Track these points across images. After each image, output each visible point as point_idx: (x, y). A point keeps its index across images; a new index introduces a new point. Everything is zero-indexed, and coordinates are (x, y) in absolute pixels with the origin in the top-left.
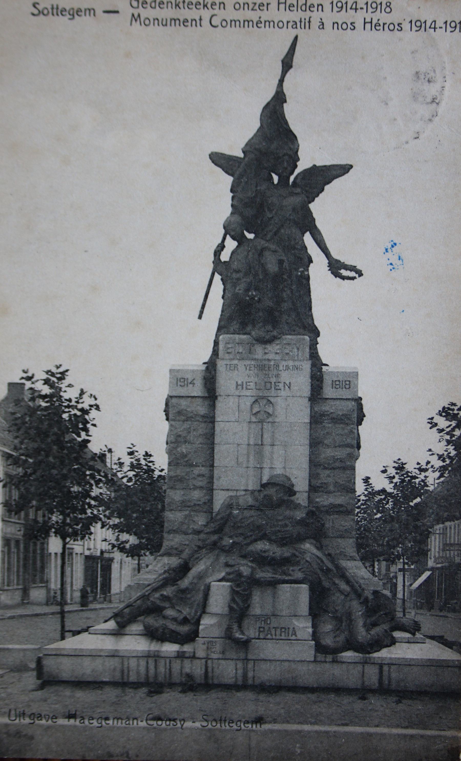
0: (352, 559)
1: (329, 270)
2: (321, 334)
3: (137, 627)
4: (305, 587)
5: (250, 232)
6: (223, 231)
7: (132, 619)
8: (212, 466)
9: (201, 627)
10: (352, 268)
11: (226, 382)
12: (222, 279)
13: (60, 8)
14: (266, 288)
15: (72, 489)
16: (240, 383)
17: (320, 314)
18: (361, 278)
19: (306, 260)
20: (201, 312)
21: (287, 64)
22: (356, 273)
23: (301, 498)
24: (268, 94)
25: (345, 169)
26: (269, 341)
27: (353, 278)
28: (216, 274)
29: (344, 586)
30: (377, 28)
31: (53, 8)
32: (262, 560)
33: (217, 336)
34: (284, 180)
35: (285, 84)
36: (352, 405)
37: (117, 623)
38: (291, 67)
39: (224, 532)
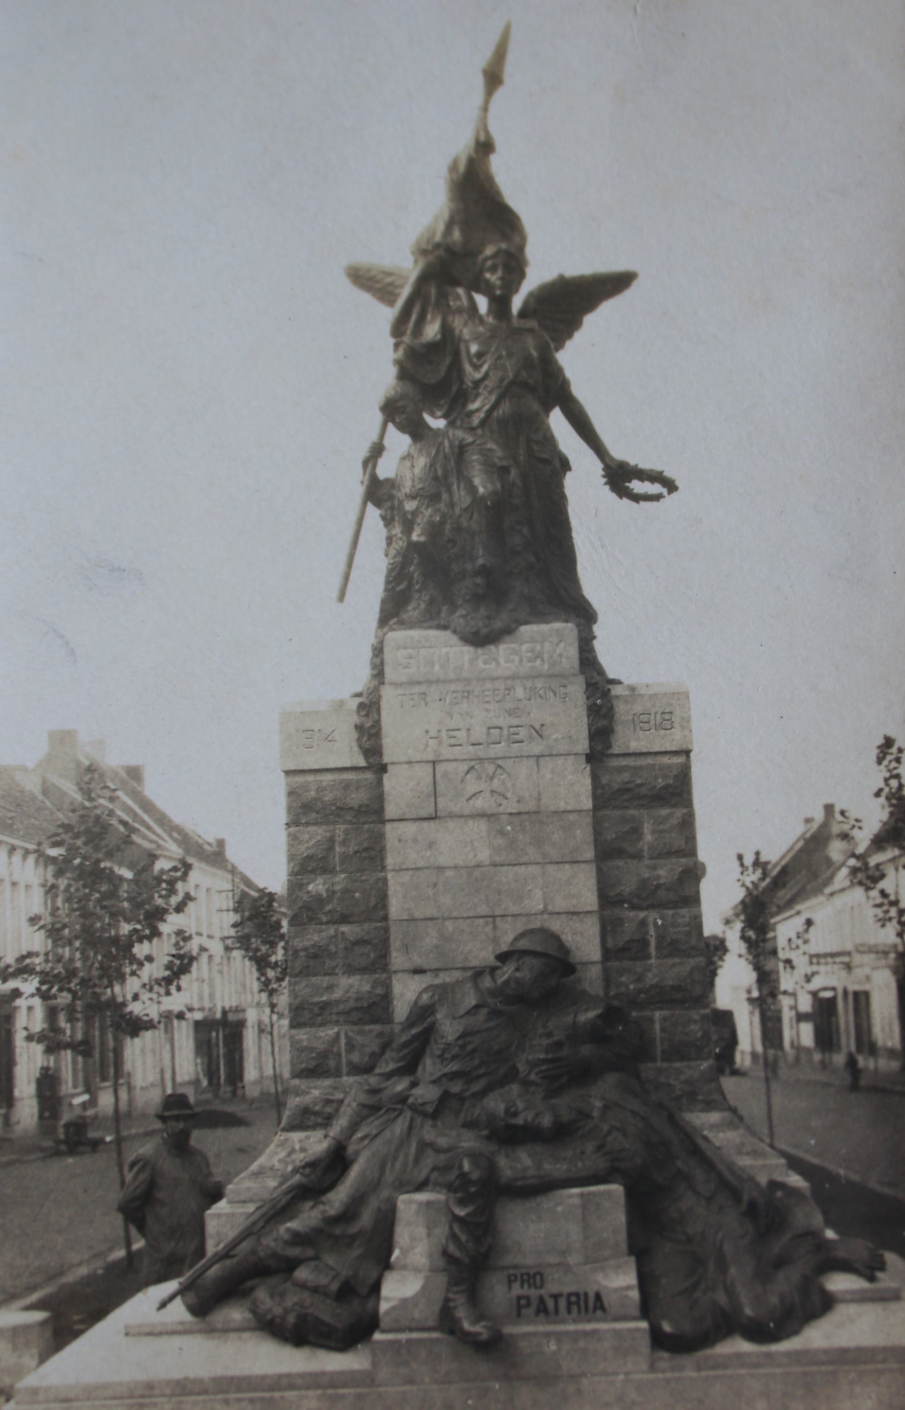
1: (606, 484)
4: (616, 1189)
6: (379, 417)
14: (490, 537)
15: (488, 275)
18: (674, 495)
21: (493, 78)
22: (664, 486)
23: (592, 979)
25: (618, 283)
27: (657, 498)
28: (370, 507)
29: (699, 1175)
32: (510, 1135)
34: (500, 305)
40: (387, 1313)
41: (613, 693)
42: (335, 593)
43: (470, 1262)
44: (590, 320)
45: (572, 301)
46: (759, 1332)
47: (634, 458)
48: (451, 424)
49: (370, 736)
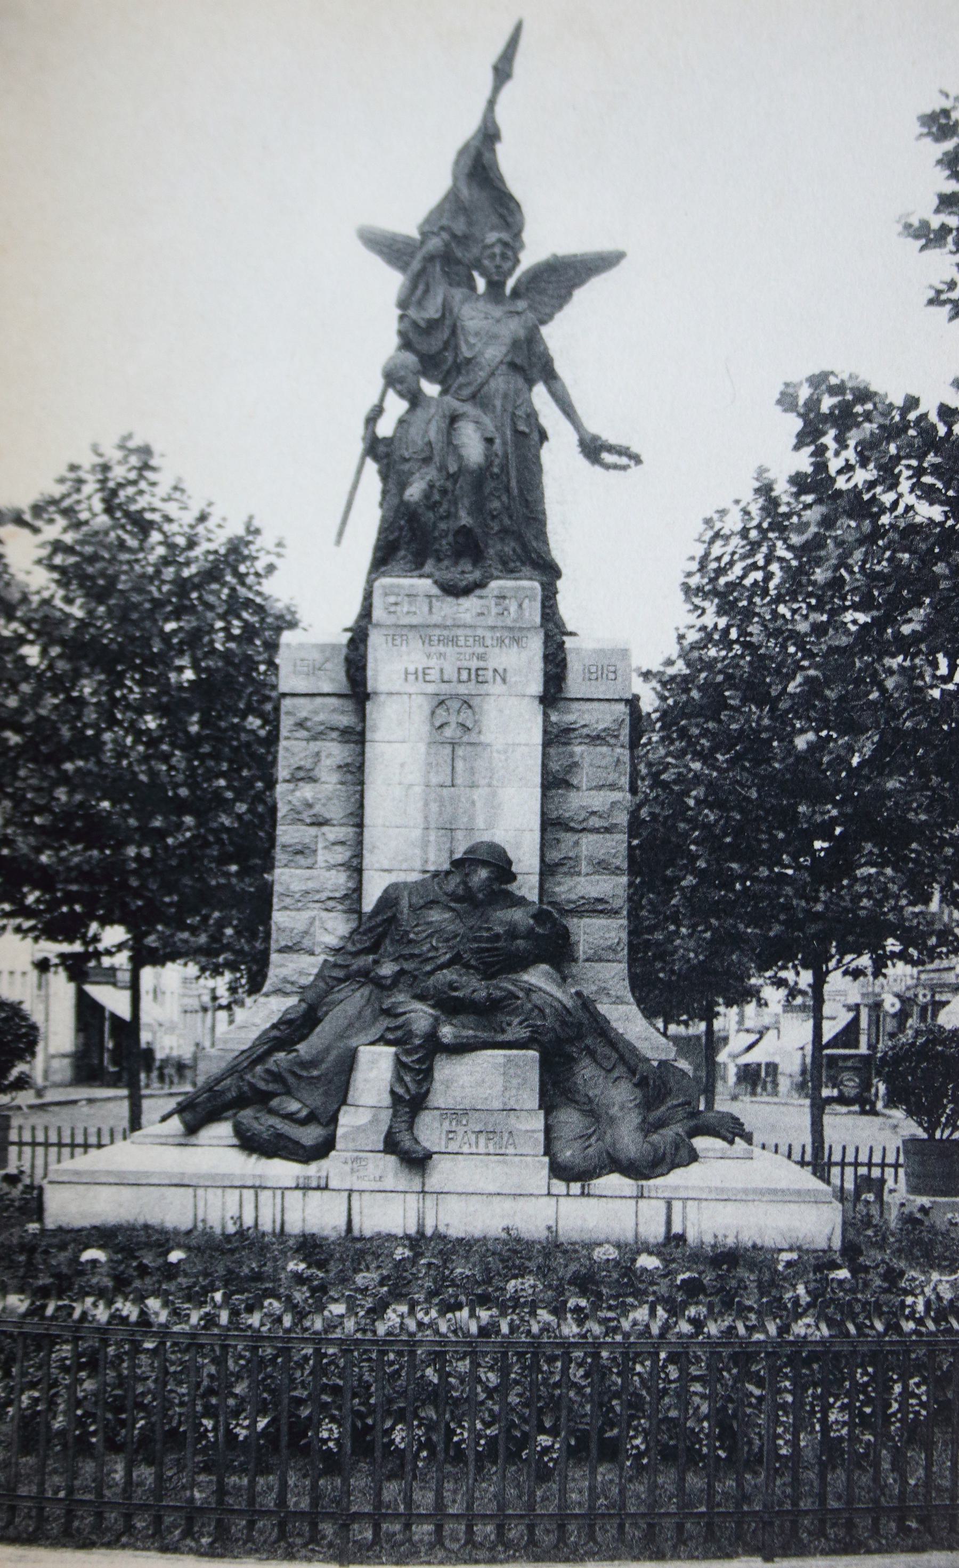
0: (619, 1001)
2: (564, 570)
3: (223, 1130)
6: (380, 382)
7: (213, 1116)
8: (360, 825)
9: (340, 1131)
11: (387, 667)
12: (380, 472)
16: (412, 669)
17: (564, 537)
19: (535, 436)
20: (340, 534)
21: (503, 71)
23: (527, 885)
24: (467, 127)
26: (466, 591)
27: (624, 468)
33: (370, 583)
36: (622, 708)
37: (184, 1122)
39: (382, 951)
40: (345, 1136)
41: (567, 646)
43: (410, 1102)
44: (580, 295)
45: (562, 278)
46: (633, 1170)
47: (610, 436)
48: (444, 392)
49: (358, 669)
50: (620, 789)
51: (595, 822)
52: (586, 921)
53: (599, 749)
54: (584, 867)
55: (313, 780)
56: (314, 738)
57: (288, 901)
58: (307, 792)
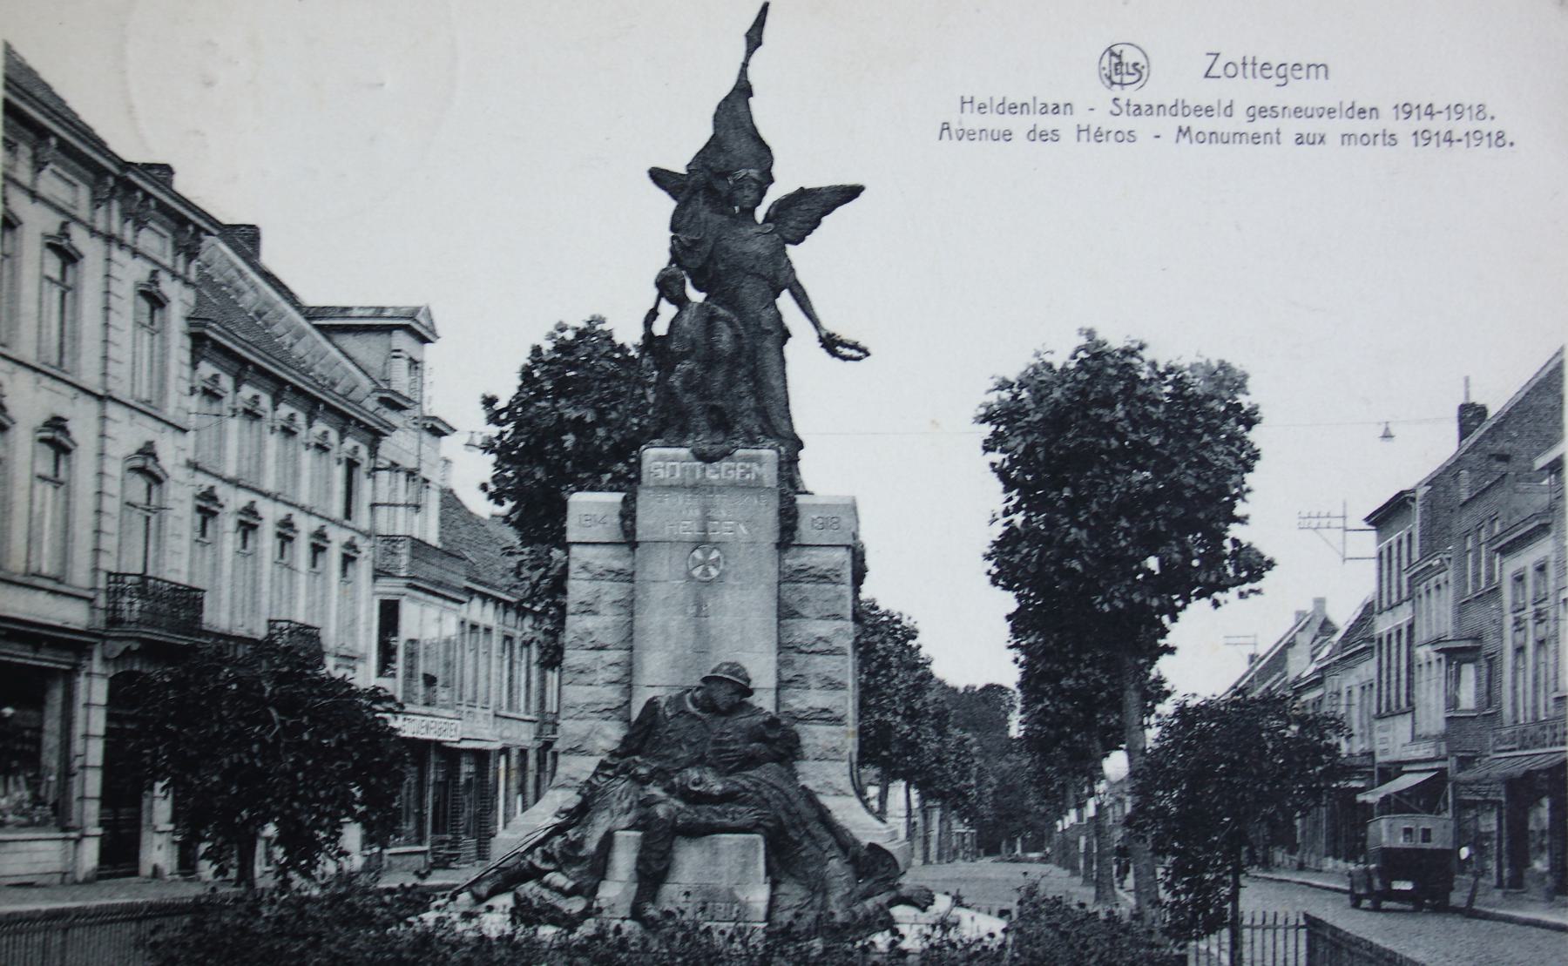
0: (840, 793)
5: (698, 288)
6: (655, 292)
10: (855, 346)
13: (1260, 62)
21: (754, 39)
23: (764, 701)
30: (1298, 74)
31: (1244, 64)
35: (750, 70)
38: (760, 44)
42: (1472, 381)
47: (846, 334)
50: (842, 618)
51: (820, 646)
52: (814, 728)
53: (822, 587)
54: (813, 682)
55: (595, 613)
56: (594, 579)
57: (572, 712)
58: (589, 622)
